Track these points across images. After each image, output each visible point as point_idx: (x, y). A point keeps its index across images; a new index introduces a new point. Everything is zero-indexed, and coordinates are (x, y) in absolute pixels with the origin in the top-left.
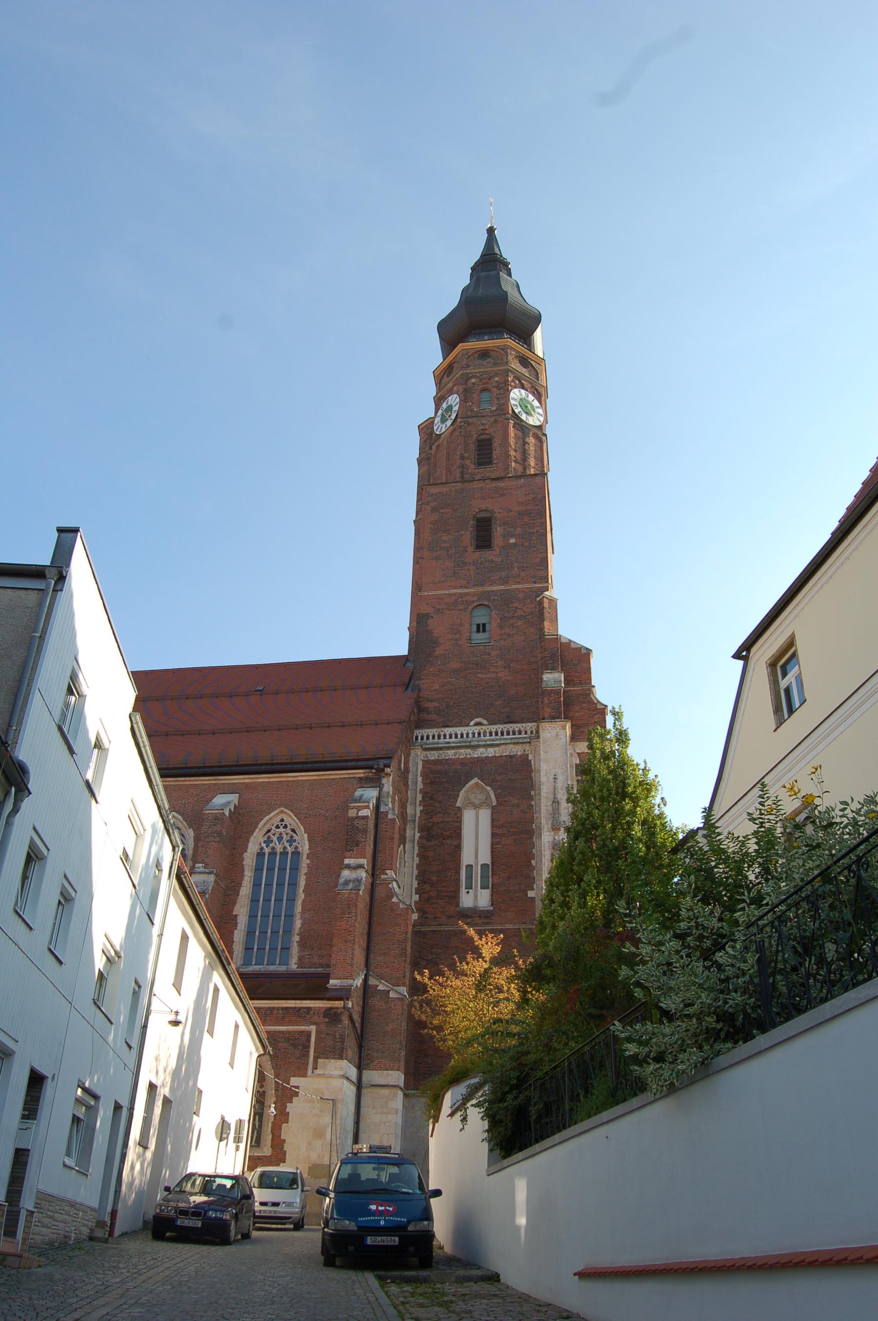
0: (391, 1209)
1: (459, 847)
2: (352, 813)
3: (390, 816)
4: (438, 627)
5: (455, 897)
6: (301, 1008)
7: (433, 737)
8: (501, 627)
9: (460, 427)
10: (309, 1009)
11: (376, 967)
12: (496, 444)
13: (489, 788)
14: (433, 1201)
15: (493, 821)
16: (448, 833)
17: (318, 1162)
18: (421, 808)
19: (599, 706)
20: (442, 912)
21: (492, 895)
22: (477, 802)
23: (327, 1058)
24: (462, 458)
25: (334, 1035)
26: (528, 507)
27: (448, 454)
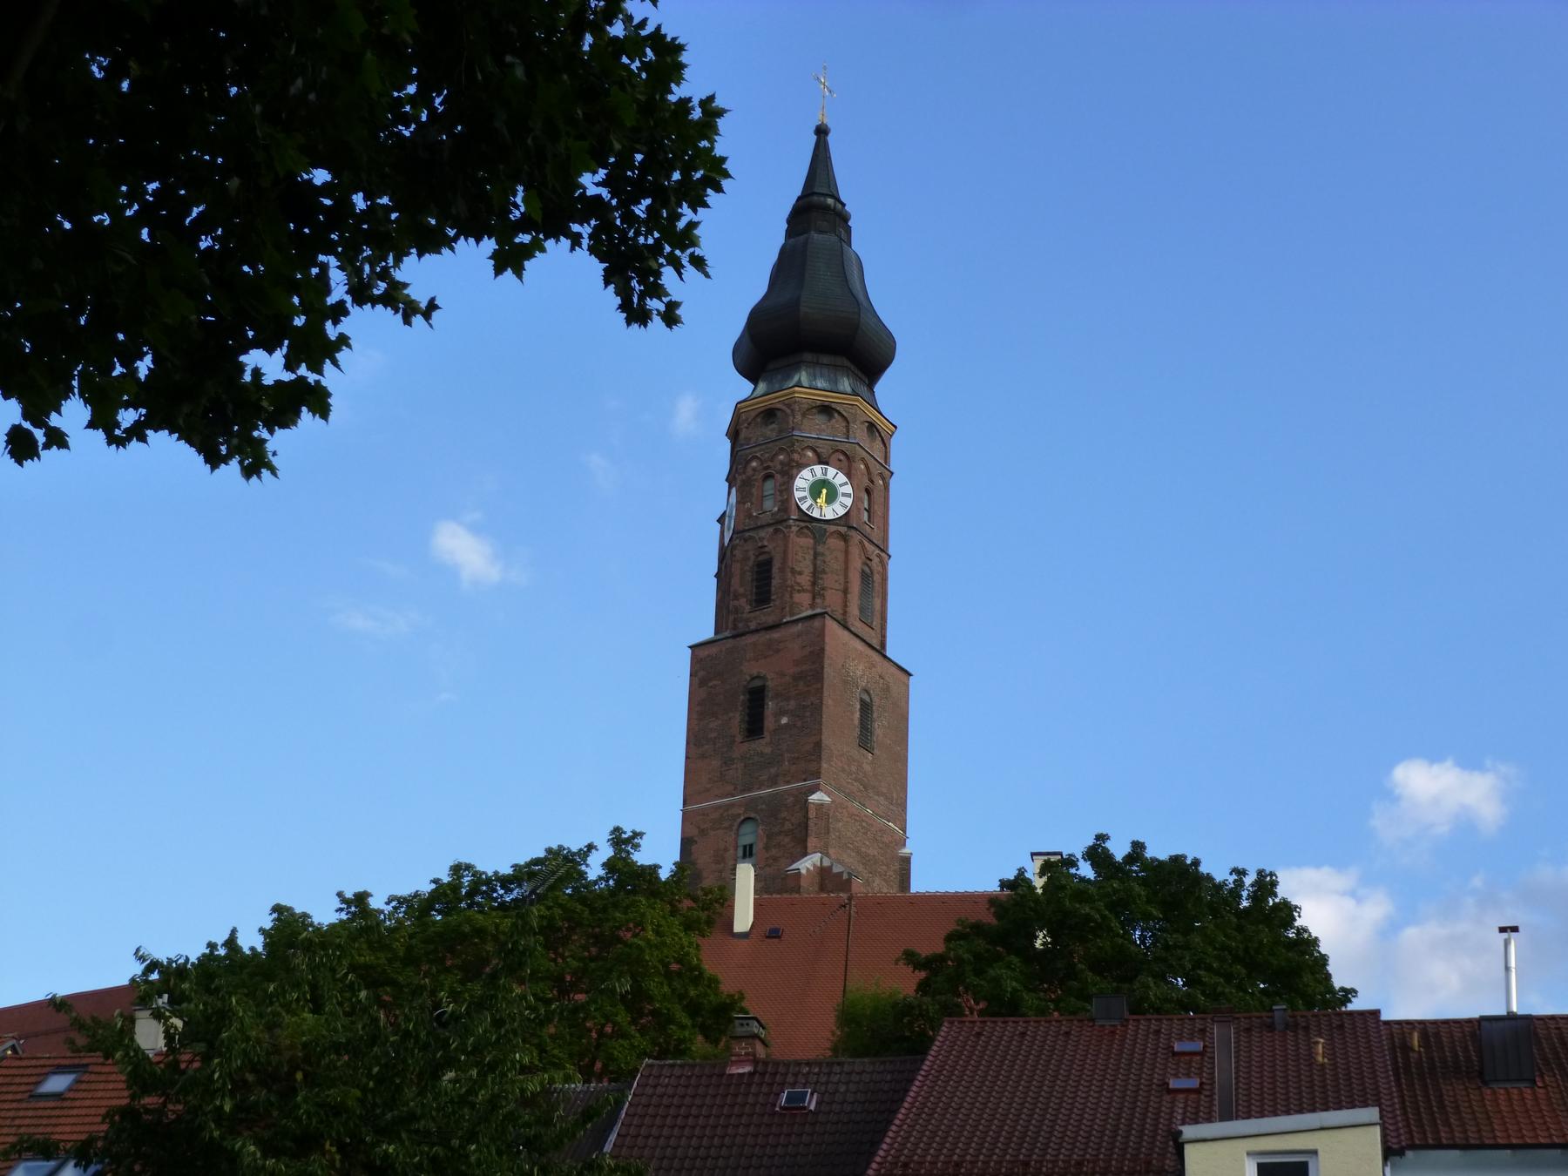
0: (67, 226)
12: (776, 565)
14: (1149, 854)
26: (805, 667)
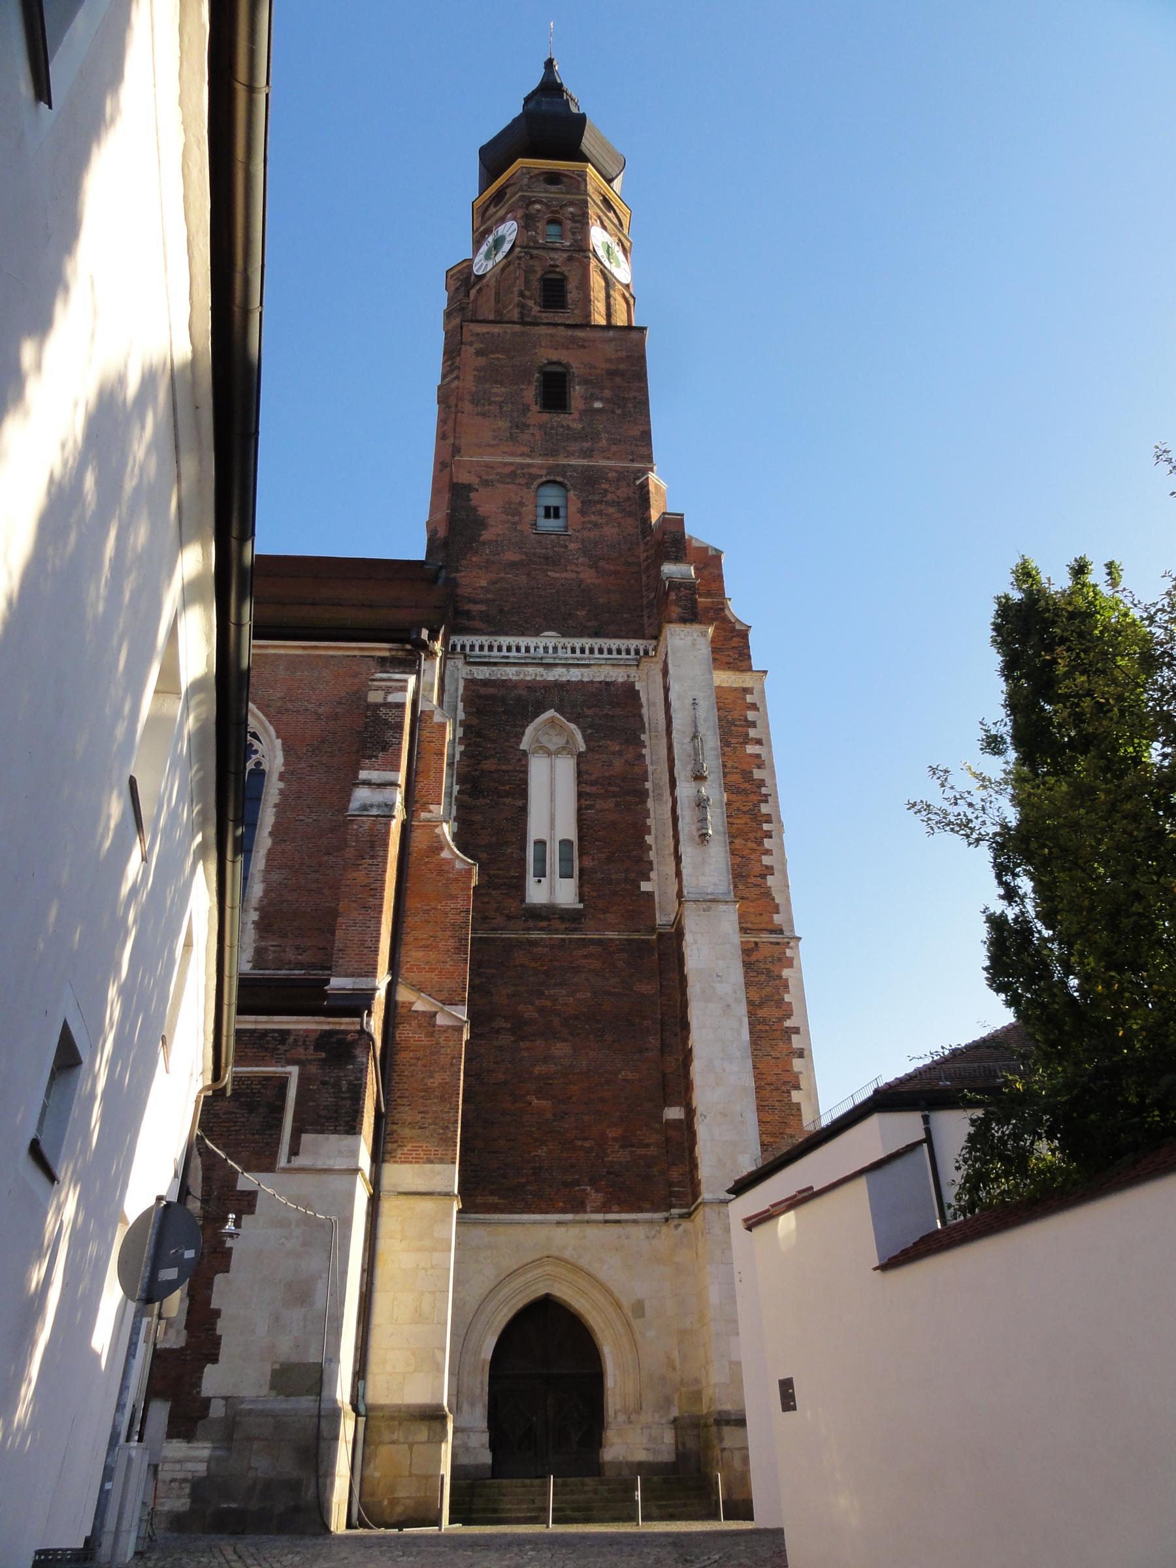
1: (523, 810)
2: (375, 697)
3: (437, 718)
4: (487, 503)
5: (518, 887)
6: (265, 1033)
7: (481, 648)
8: (582, 512)
9: (519, 258)
10: (284, 1034)
11: (409, 970)
12: (572, 285)
13: (573, 726)
15: (579, 774)
16: (507, 788)
17: (295, 1359)
18: (462, 748)
19: (738, 627)
20: (497, 909)
21: (581, 886)
22: (552, 748)
23: (322, 1132)
24: (521, 294)
25: (337, 1085)
27: (497, 294)
